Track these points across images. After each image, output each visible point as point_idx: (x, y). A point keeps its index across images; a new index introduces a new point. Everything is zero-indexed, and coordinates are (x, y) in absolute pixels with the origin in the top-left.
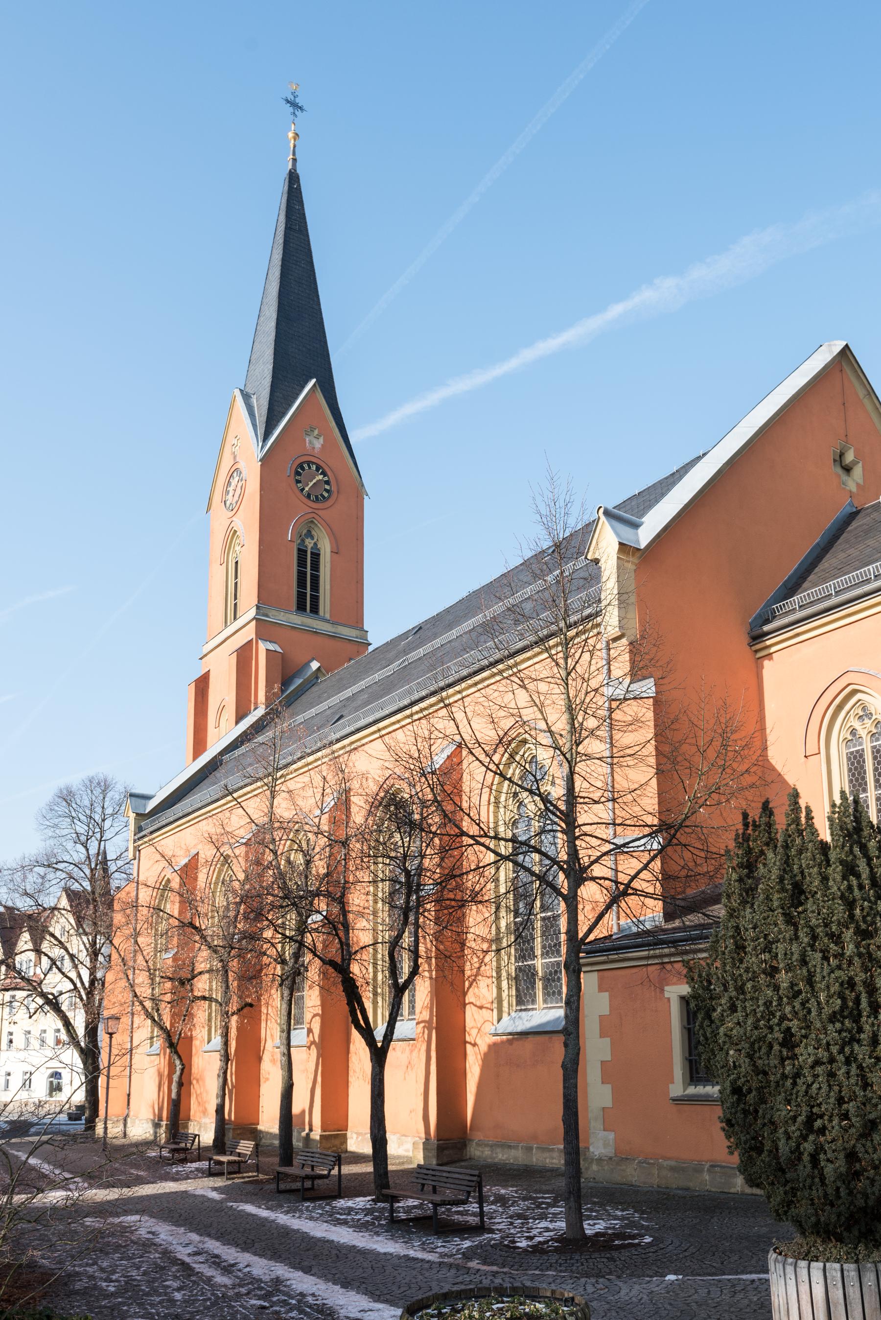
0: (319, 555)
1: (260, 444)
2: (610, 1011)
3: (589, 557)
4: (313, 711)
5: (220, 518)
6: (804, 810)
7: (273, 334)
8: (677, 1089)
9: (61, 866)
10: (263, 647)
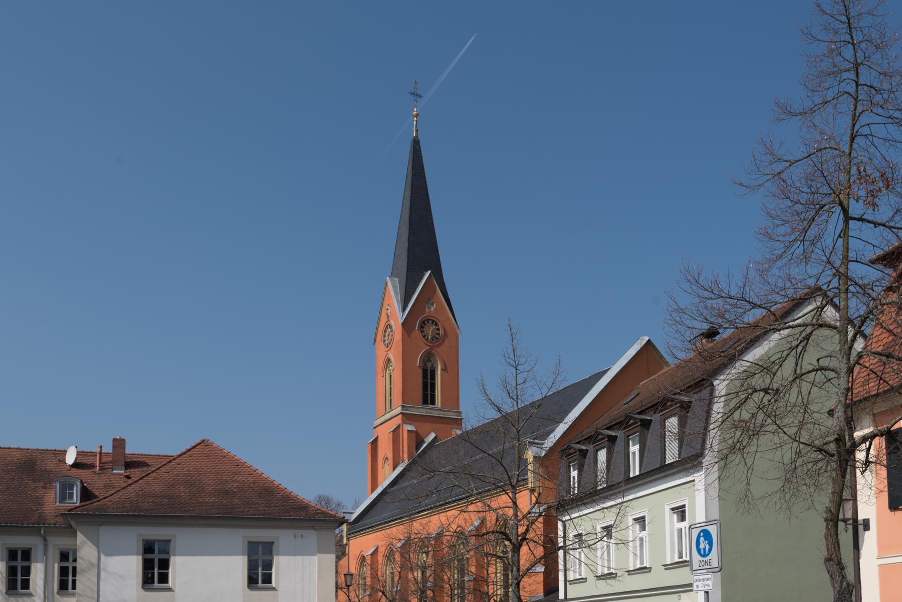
1: (402, 314)
5: (381, 350)
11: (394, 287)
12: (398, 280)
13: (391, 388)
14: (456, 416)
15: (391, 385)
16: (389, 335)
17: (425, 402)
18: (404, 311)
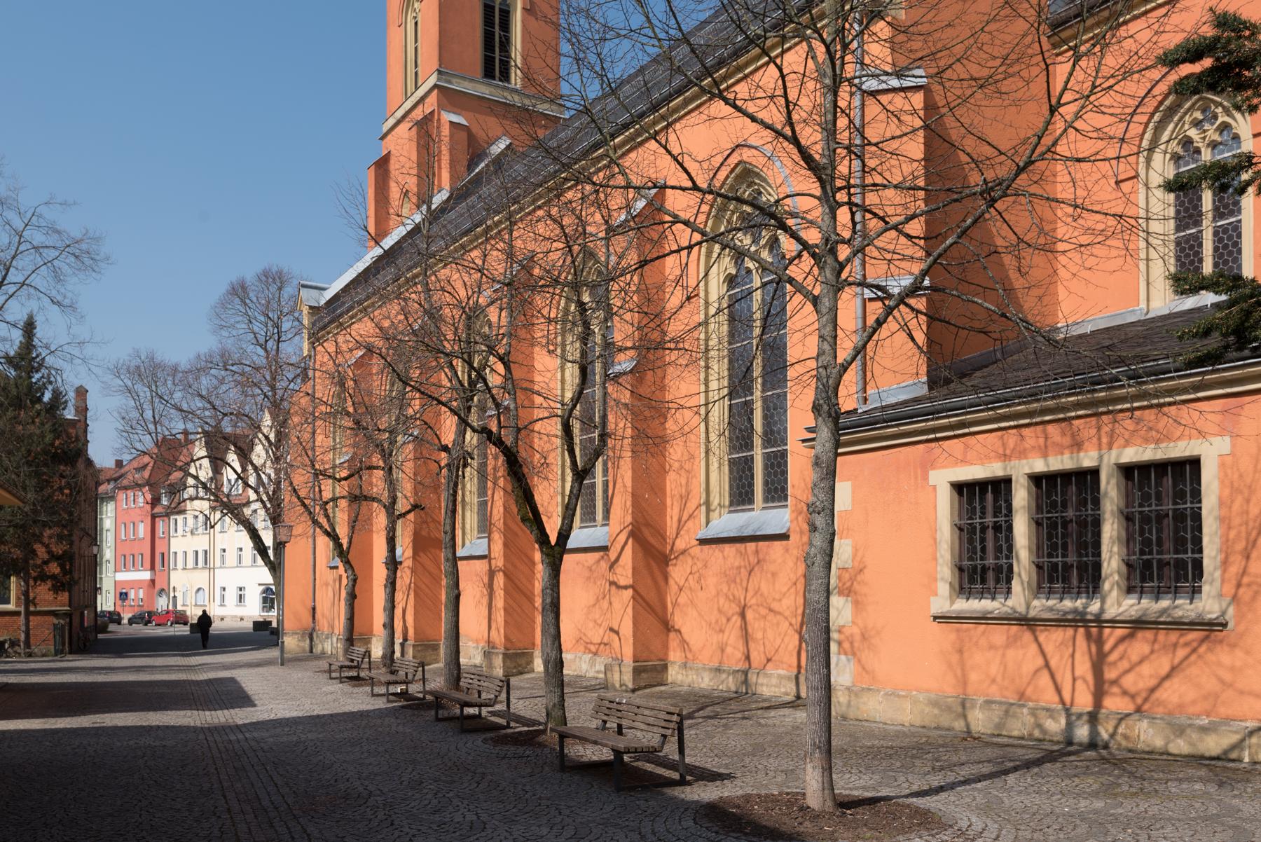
0: (508, 12)
2: (853, 505)
8: (943, 600)
10: (449, 117)
15: (416, 42)
17: (489, 73)
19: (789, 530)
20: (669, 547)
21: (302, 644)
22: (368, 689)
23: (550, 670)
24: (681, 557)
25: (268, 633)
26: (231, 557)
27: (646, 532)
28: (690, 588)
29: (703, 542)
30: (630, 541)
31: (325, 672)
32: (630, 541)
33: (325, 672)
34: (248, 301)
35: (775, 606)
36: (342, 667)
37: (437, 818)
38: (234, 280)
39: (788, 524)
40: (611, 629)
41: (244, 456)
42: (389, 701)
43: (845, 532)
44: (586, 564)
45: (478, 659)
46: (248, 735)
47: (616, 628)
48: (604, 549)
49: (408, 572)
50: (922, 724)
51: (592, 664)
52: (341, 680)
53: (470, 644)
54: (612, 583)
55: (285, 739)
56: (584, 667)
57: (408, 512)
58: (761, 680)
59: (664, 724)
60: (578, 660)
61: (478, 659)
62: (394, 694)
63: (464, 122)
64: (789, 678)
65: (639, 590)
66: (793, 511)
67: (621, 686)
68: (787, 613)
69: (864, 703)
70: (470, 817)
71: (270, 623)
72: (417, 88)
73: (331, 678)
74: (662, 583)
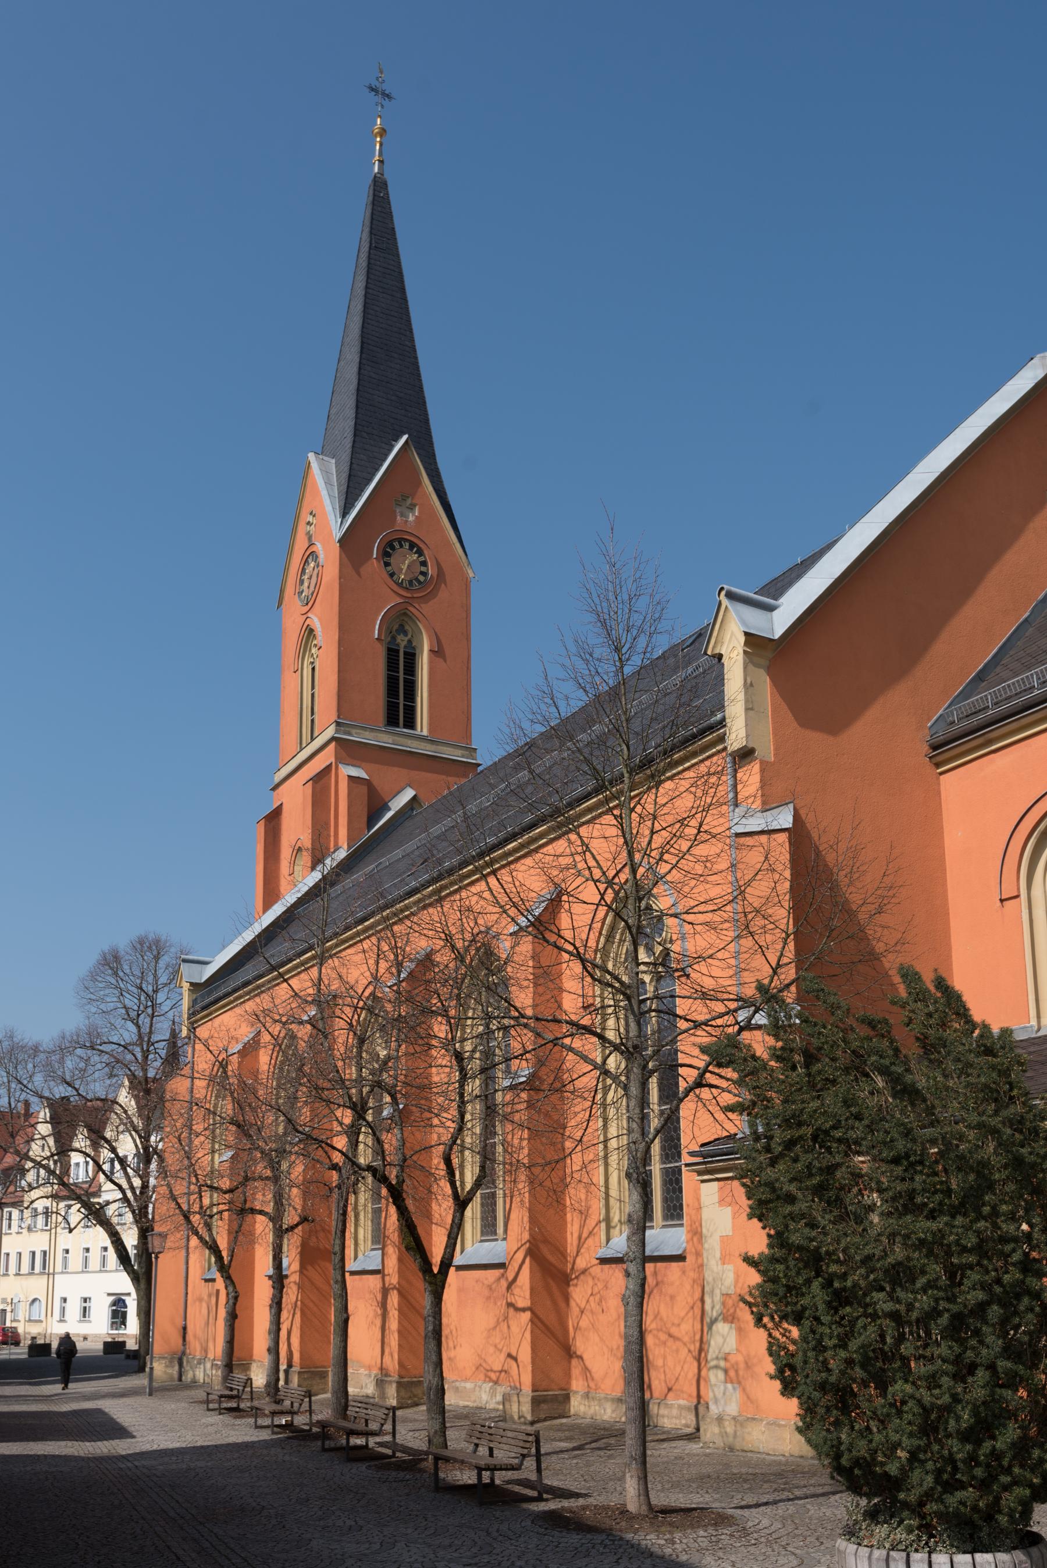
1: (339, 520)
2: (733, 1231)
3: (709, 652)
4: (399, 853)
6: (897, 979)
7: (355, 382)
9: (105, 1048)
11: (325, 473)
12: (333, 461)
13: (313, 695)
14: (463, 756)
15: (313, 688)
16: (310, 578)
17: (392, 720)
18: (344, 514)
19: (685, 1251)
20: (569, 1266)
21: (170, 1371)
22: (251, 1421)
23: (432, 1397)
24: (582, 1277)
25: (123, 1356)
26: (75, 1261)
27: (545, 1251)
28: (592, 1312)
29: (604, 1261)
30: (528, 1260)
31: (201, 1402)
32: (528, 1260)
33: (201, 1402)
34: (121, 974)
35: (674, 1331)
36: (221, 1396)
37: (322, 1523)
38: (106, 948)
39: (684, 1245)
40: (509, 1356)
41: (97, 1137)
42: (273, 1433)
43: (727, 1257)
44: (486, 1282)
45: (370, 1389)
46: (136, 1463)
47: (514, 1354)
48: (502, 1266)
49: (295, 1288)
50: (801, 1454)
51: (493, 1394)
52: (221, 1411)
53: (362, 1371)
54: (510, 1305)
55: (174, 1466)
56: (485, 1397)
57: (297, 1225)
58: (662, 1412)
59: (522, 1444)
60: (477, 1389)
61: (370, 1389)
62: (280, 1426)
63: (364, 775)
64: (688, 1409)
65: (538, 1313)
66: (688, 1232)
67: (519, 1418)
68: (686, 1339)
69: (749, 1433)
70: (349, 1523)
71: (124, 1343)
72: (312, 739)
73: (209, 1410)
74: (562, 1305)
